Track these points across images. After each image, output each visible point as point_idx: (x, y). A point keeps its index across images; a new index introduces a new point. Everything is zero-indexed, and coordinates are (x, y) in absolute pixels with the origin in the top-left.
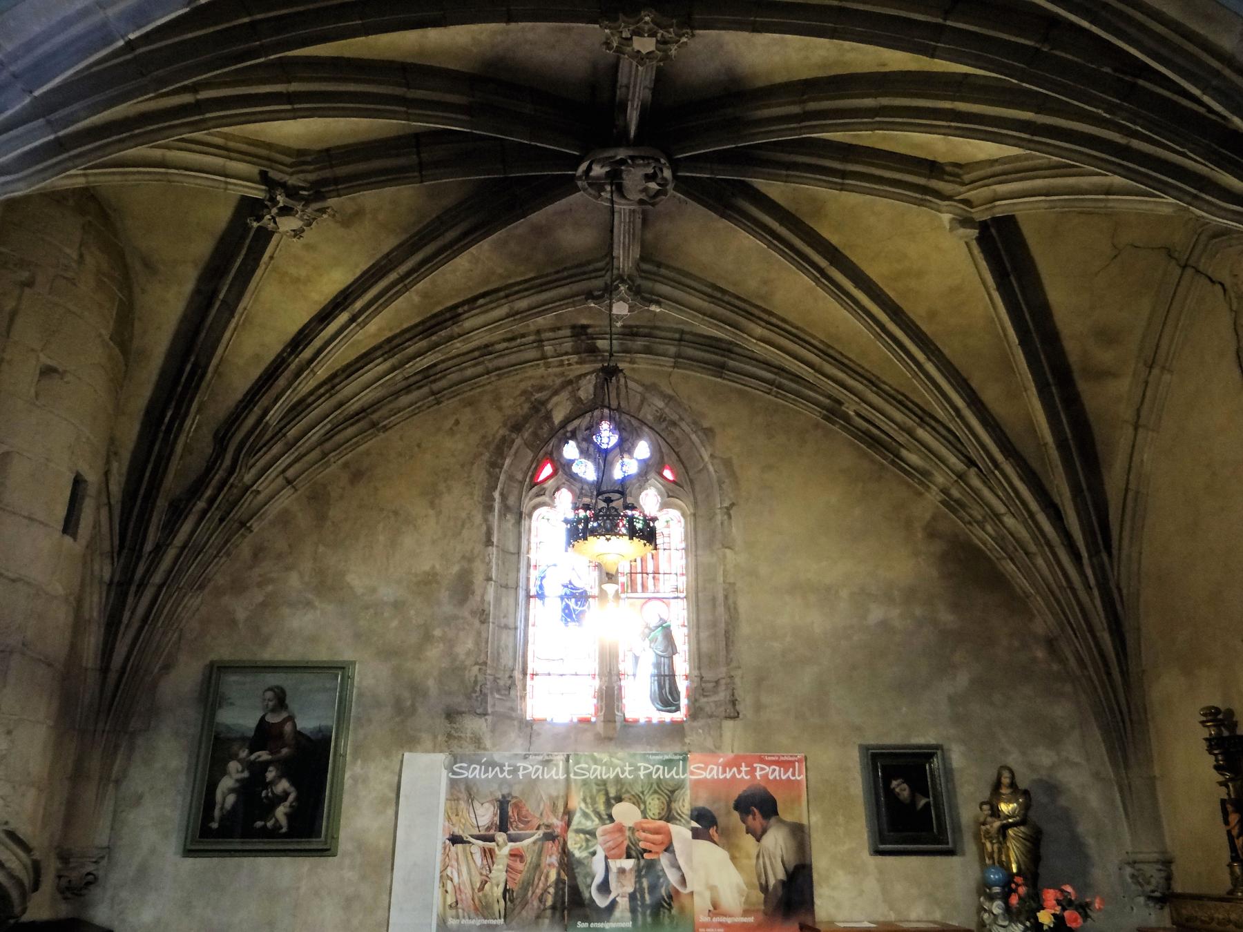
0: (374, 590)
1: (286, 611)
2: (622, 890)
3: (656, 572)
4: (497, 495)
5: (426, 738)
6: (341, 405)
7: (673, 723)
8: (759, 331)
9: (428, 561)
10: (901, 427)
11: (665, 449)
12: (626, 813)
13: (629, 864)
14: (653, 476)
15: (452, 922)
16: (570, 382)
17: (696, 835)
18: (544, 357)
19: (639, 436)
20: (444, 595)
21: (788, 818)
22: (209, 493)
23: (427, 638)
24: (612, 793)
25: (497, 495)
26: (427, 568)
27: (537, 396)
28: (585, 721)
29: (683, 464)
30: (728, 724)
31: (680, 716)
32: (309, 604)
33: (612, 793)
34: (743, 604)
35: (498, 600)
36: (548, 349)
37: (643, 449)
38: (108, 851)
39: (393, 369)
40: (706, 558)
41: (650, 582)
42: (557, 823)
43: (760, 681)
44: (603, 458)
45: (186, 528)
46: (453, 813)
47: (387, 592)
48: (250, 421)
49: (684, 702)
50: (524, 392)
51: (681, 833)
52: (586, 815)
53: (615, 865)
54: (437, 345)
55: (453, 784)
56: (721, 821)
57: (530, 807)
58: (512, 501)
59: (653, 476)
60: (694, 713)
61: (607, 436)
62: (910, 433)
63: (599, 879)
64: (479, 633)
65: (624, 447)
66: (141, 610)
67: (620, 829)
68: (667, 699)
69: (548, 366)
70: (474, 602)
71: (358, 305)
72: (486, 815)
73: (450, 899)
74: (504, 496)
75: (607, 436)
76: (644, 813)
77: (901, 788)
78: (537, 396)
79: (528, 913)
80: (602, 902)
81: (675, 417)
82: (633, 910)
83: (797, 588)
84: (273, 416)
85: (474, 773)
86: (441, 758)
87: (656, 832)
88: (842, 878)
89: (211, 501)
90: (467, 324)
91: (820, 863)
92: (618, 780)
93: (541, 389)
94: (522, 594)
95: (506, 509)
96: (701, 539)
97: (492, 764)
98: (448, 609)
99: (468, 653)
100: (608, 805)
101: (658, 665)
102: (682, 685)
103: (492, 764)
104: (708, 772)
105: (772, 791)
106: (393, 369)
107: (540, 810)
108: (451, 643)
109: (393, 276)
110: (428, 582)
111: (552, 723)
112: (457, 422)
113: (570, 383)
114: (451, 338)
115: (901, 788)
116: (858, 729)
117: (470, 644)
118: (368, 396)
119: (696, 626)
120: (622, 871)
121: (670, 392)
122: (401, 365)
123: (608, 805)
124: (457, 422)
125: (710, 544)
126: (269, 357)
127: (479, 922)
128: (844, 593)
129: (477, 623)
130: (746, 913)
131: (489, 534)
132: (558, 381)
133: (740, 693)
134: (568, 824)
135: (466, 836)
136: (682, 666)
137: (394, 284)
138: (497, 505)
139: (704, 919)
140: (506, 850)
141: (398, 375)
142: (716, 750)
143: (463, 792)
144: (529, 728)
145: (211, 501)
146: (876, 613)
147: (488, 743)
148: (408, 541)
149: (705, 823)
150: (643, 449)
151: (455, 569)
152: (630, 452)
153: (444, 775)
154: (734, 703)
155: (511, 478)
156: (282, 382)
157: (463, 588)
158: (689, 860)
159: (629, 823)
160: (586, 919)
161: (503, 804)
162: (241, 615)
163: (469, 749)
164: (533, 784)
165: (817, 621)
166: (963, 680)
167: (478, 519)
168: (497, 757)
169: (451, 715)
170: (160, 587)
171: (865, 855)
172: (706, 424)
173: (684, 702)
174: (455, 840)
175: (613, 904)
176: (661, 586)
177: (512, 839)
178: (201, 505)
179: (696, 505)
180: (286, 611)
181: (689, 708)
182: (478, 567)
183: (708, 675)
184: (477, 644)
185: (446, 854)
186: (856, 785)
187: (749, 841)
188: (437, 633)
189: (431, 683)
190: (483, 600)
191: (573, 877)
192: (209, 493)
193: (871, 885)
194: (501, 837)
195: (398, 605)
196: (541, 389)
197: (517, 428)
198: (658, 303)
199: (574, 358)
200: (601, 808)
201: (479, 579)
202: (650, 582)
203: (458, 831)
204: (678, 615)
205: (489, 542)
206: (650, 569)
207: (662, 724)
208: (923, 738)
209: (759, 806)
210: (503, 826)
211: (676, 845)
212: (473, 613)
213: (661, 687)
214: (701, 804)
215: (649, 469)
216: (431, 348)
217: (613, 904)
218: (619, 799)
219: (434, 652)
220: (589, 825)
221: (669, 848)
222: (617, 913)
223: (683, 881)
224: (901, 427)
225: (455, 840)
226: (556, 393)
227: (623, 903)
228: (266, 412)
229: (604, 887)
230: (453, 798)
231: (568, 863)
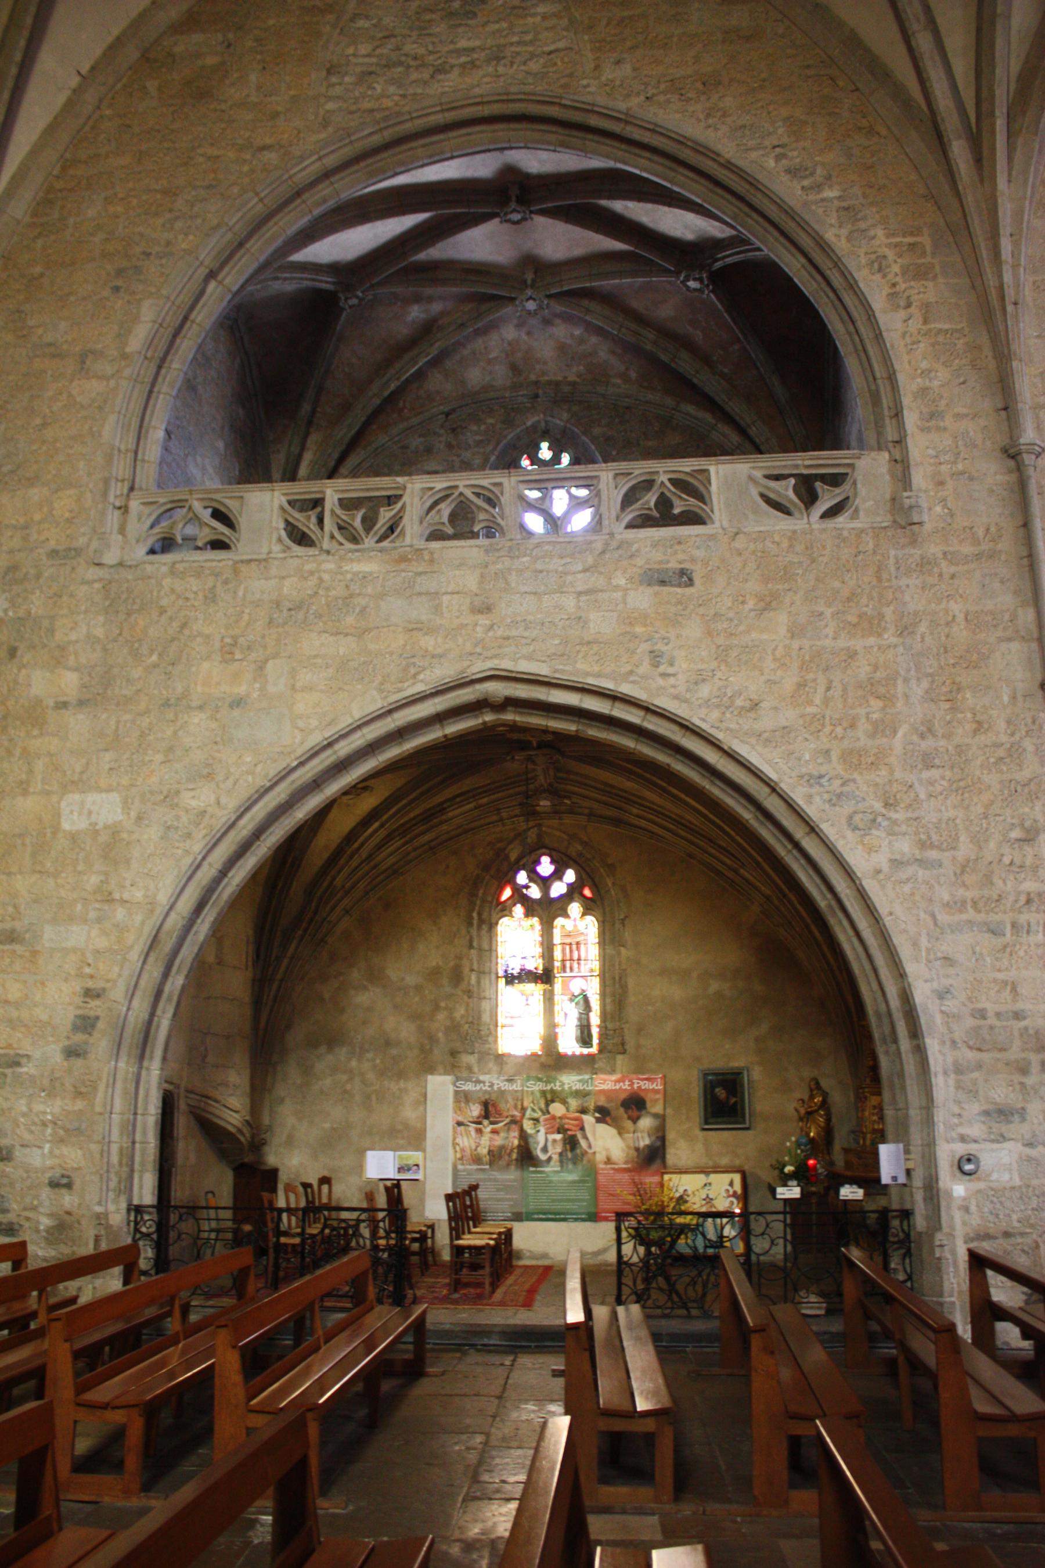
0: (403, 979)
1: (352, 992)
2: (554, 1151)
3: (579, 959)
4: (475, 915)
5: (441, 1069)
6: (376, 866)
7: (589, 1055)
8: (635, 811)
9: (434, 960)
10: (730, 868)
11: (584, 876)
12: (557, 1109)
13: (559, 1137)
14: (576, 896)
15: (460, 1167)
16: (520, 834)
17: (598, 1121)
18: (502, 820)
19: (568, 867)
20: (445, 981)
21: (654, 1110)
22: (304, 925)
23: (437, 1008)
24: (549, 1097)
25: (475, 915)
26: (434, 964)
27: (499, 845)
28: (534, 1055)
29: (595, 887)
30: (619, 1057)
31: (594, 1050)
32: (365, 988)
33: (549, 1097)
34: (631, 982)
35: (479, 982)
36: (504, 815)
37: (570, 876)
38: (269, 1128)
39: (406, 843)
40: (610, 950)
41: (575, 965)
42: (517, 1114)
43: (640, 1030)
44: (545, 883)
45: (293, 946)
46: (458, 1109)
47: (411, 980)
48: (325, 884)
49: (595, 1041)
50: (490, 843)
51: (589, 1120)
52: (533, 1110)
53: (551, 1137)
54: (432, 827)
55: (456, 1093)
56: (613, 1113)
57: (502, 1106)
58: (485, 916)
59: (576, 896)
60: (600, 1051)
61: (546, 867)
62: (736, 872)
63: (541, 1145)
64: (468, 1005)
65: (558, 875)
66: (273, 993)
67: (554, 1118)
68: (585, 1039)
69: (504, 825)
70: (464, 985)
71: (385, 817)
72: (476, 1110)
73: (459, 1155)
74: (480, 914)
75: (546, 867)
76: (568, 1109)
77: (721, 1093)
78: (499, 845)
79: (503, 1162)
80: (543, 1157)
81: (589, 856)
82: (561, 1162)
83: (664, 972)
84: (338, 882)
85: (469, 1087)
86: (449, 1078)
87: (575, 1119)
88: (682, 1144)
89: (305, 931)
90: (451, 814)
91: (671, 1136)
92: (552, 1091)
93: (501, 840)
94: (493, 976)
95: (481, 921)
96: (607, 937)
97: (478, 1082)
98: (448, 989)
99: (462, 1017)
100: (547, 1105)
101: (580, 1019)
102: (595, 1031)
103: (478, 1082)
104: (607, 1083)
105: (642, 1094)
106: (406, 843)
107: (508, 1108)
108: (450, 1010)
109: (405, 802)
110: (434, 974)
111: (515, 1057)
112: (447, 867)
113: (520, 836)
114: (441, 823)
115: (721, 1093)
116: (698, 1059)
117: (462, 1011)
118: (391, 860)
119: (603, 995)
120: (554, 1141)
121: (585, 839)
122: (411, 840)
123: (547, 1105)
124: (447, 867)
125: (612, 941)
126: (333, 846)
127: (475, 1167)
128: (695, 974)
129: (465, 997)
130: (626, 1163)
131: (471, 941)
132: (512, 834)
133: (627, 1038)
134: (524, 1115)
135: (466, 1122)
136: (595, 1019)
137: (405, 806)
138: (475, 922)
139: (602, 1166)
140: (489, 1129)
141: (409, 847)
142: (613, 1071)
143: (462, 1098)
144: (501, 1059)
145: (305, 931)
146: (714, 986)
147: (476, 1069)
148: (421, 947)
149: (604, 1115)
150: (570, 876)
151: (452, 963)
152: (560, 878)
153: (451, 1089)
154: (623, 1044)
155: (484, 901)
156: (342, 861)
157: (457, 976)
158: (594, 1134)
159: (559, 1114)
160: (535, 1166)
161: (486, 1104)
162: (327, 996)
163: (465, 1074)
164: (502, 1093)
165: (676, 992)
166: (764, 1027)
167: (463, 931)
168: (482, 1078)
169: (454, 1054)
170: (282, 981)
171: (697, 1131)
172: (610, 861)
173: (595, 1041)
174: (459, 1124)
175: (550, 1159)
176: (582, 967)
177: (492, 1123)
178: (300, 932)
179: (604, 914)
180: (352, 992)
181: (600, 1044)
182: (465, 962)
183: (610, 1026)
184: (467, 1010)
185: (455, 1132)
186: (696, 1092)
187: (629, 1124)
188: (443, 1004)
189: (440, 1035)
190: (469, 984)
191: (527, 1143)
192: (304, 925)
193: (699, 1147)
194: (486, 1122)
195: (418, 988)
196: (501, 840)
197: (486, 868)
198: (569, 798)
199: (522, 819)
200: (543, 1106)
201: (466, 971)
202: (575, 965)
203: (460, 1119)
204: (593, 989)
205: (471, 947)
206: (576, 956)
207: (582, 1055)
208: (736, 1064)
209: (635, 1104)
210: (486, 1115)
211: (587, 1127)
212: (464, 992)
213: (582, 1033)
214: (600, 1104)
215: (574, 891)
216: (428, 830)
217: (550, 1159)
218: (553, 1101)
219: (441, 1016)
220: (535, 1115)
221: (582, 1129)
222: (552, 1163)
223: (590, 1147)
224: (730, 868)
225: (459, 1124)
226: (510, 842)
227: (556, 1157)
228: (334, 878)
229: (545, 1150)
230: (457, 1100)
231: (524, 1136)
